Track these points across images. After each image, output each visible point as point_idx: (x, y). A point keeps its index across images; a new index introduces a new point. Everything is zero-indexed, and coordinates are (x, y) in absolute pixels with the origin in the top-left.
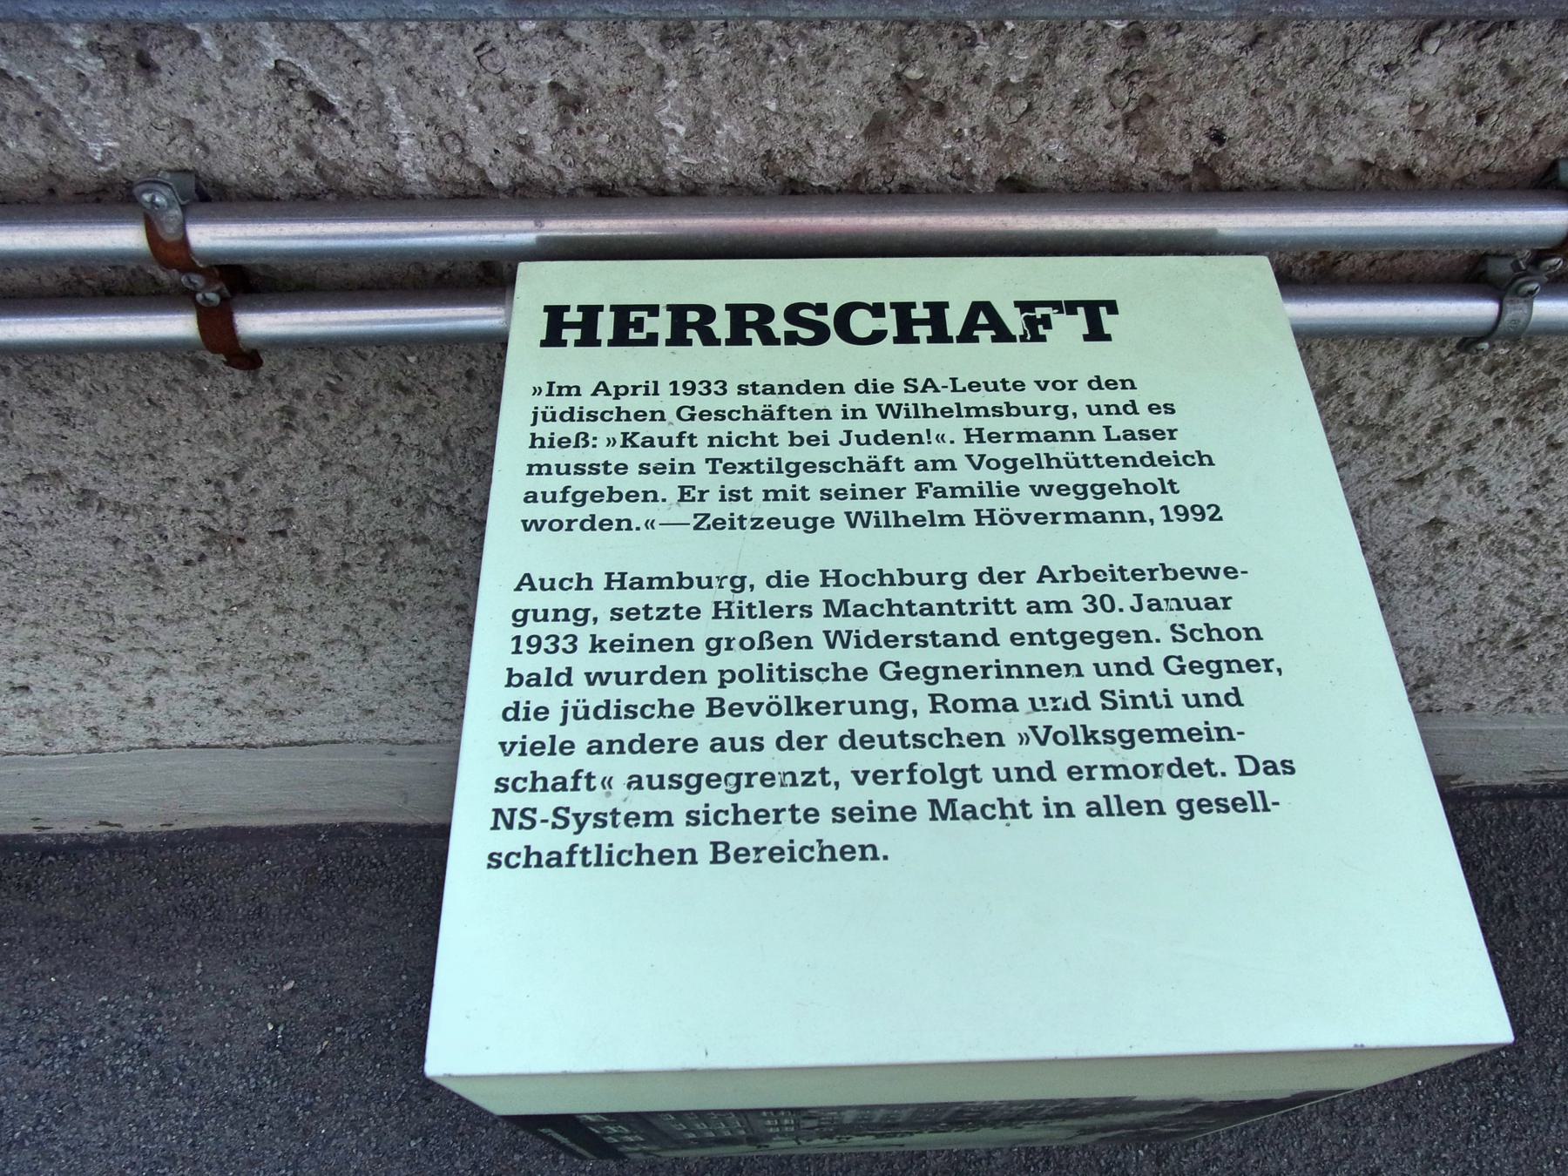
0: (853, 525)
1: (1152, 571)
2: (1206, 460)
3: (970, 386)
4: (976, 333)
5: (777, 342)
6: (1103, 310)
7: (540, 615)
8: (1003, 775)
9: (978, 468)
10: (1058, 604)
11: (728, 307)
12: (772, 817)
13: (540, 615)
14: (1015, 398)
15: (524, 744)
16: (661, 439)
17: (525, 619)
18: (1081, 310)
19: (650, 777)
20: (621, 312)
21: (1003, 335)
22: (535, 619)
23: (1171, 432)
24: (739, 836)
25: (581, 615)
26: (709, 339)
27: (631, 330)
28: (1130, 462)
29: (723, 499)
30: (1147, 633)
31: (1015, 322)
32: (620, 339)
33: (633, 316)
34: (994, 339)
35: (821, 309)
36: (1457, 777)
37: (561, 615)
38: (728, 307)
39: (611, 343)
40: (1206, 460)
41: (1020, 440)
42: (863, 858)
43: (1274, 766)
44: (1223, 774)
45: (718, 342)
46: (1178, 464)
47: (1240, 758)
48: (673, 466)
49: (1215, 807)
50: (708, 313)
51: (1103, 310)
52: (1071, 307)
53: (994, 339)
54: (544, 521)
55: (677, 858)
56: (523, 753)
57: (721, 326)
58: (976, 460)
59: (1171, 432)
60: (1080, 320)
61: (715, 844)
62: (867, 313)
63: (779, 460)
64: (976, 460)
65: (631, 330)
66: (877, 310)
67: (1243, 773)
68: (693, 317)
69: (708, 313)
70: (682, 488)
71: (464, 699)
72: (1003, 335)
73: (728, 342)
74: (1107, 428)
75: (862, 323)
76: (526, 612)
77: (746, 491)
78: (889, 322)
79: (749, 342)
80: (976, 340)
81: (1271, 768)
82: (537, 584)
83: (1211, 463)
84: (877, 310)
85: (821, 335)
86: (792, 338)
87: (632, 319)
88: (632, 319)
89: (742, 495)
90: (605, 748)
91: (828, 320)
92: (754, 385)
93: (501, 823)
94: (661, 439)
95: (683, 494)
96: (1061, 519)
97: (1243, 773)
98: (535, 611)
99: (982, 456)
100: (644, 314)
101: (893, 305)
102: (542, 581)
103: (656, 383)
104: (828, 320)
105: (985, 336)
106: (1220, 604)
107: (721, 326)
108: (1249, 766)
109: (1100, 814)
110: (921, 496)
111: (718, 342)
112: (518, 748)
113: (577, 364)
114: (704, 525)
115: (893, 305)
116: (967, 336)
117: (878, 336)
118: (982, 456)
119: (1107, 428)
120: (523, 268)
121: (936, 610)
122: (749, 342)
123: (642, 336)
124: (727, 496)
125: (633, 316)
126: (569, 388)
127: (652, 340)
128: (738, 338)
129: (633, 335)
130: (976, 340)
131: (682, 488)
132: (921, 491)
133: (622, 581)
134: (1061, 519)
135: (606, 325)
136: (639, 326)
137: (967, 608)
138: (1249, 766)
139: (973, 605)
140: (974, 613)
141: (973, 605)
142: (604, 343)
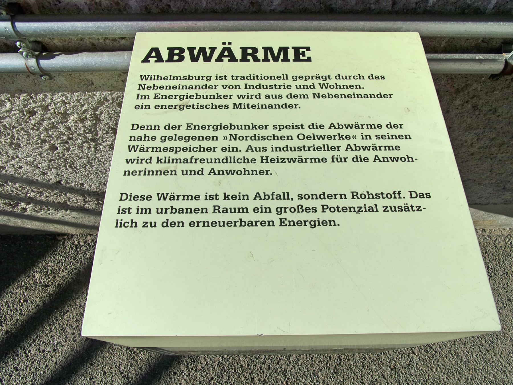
1: (334, 136)
4: (223, 58)
8: (185, 173)
10: (389, 147)
11: (263, 48)
12: (303, 224)
16: (272, 95)
19: (231, 209)
20: (296, 49)
21: (233, 59)
26: (256, 59)
27: (301, 56)
31: (238, 55)
32: (297, 59)
33: (301, 51)
34: (229, 61)
38: (263, 48)
39: (294, 60)
42: (269, 225)
43: (423, 195)
44: (404, 198)
45: (259, 61)
47: (410, 192)
48: (259, 105)
49: (311, 210)
50: (255, 50)
53: (229, 61)
54: (226, 86)
55: (267, 224)
57: (260, 55)
61: (214, 206)
65: (301, 56)
67: (411, 197)
68: (250, 51)
69: (255, 50)
72: (233, 59)
73: (241, 61)
79: (248, 61)
80: (222, 61)
81: (422, 196)
82: (254, 149)
87: (301, 52)
88: (301, 52)
90: (185, 211)
94: (272, 95)
96: (309, 161)
97: (411, 197)
100: (305, 50)
102: (256, 148)
103: (287, 75)
105: (226, 59)
107: (260, 55)
108: (414, 195)
109: (373, 211)
111: (259, 61)
113: (154, 68)
120: (138, 34)
121: (274, 107)
122: (248, 61)
123: (305, 58)
125: (301, 51)
126: (177, 77)
128: (244, 59)
129: (302, 57)
130: (222, 61)
133: (267, 160)
134: (309, 161)
135: (291, 54)
136: (303, 54)
137: (307, 149)
138: (414, 195)
139: (280, 86)
140: (309, 150)
141: (280, 86)
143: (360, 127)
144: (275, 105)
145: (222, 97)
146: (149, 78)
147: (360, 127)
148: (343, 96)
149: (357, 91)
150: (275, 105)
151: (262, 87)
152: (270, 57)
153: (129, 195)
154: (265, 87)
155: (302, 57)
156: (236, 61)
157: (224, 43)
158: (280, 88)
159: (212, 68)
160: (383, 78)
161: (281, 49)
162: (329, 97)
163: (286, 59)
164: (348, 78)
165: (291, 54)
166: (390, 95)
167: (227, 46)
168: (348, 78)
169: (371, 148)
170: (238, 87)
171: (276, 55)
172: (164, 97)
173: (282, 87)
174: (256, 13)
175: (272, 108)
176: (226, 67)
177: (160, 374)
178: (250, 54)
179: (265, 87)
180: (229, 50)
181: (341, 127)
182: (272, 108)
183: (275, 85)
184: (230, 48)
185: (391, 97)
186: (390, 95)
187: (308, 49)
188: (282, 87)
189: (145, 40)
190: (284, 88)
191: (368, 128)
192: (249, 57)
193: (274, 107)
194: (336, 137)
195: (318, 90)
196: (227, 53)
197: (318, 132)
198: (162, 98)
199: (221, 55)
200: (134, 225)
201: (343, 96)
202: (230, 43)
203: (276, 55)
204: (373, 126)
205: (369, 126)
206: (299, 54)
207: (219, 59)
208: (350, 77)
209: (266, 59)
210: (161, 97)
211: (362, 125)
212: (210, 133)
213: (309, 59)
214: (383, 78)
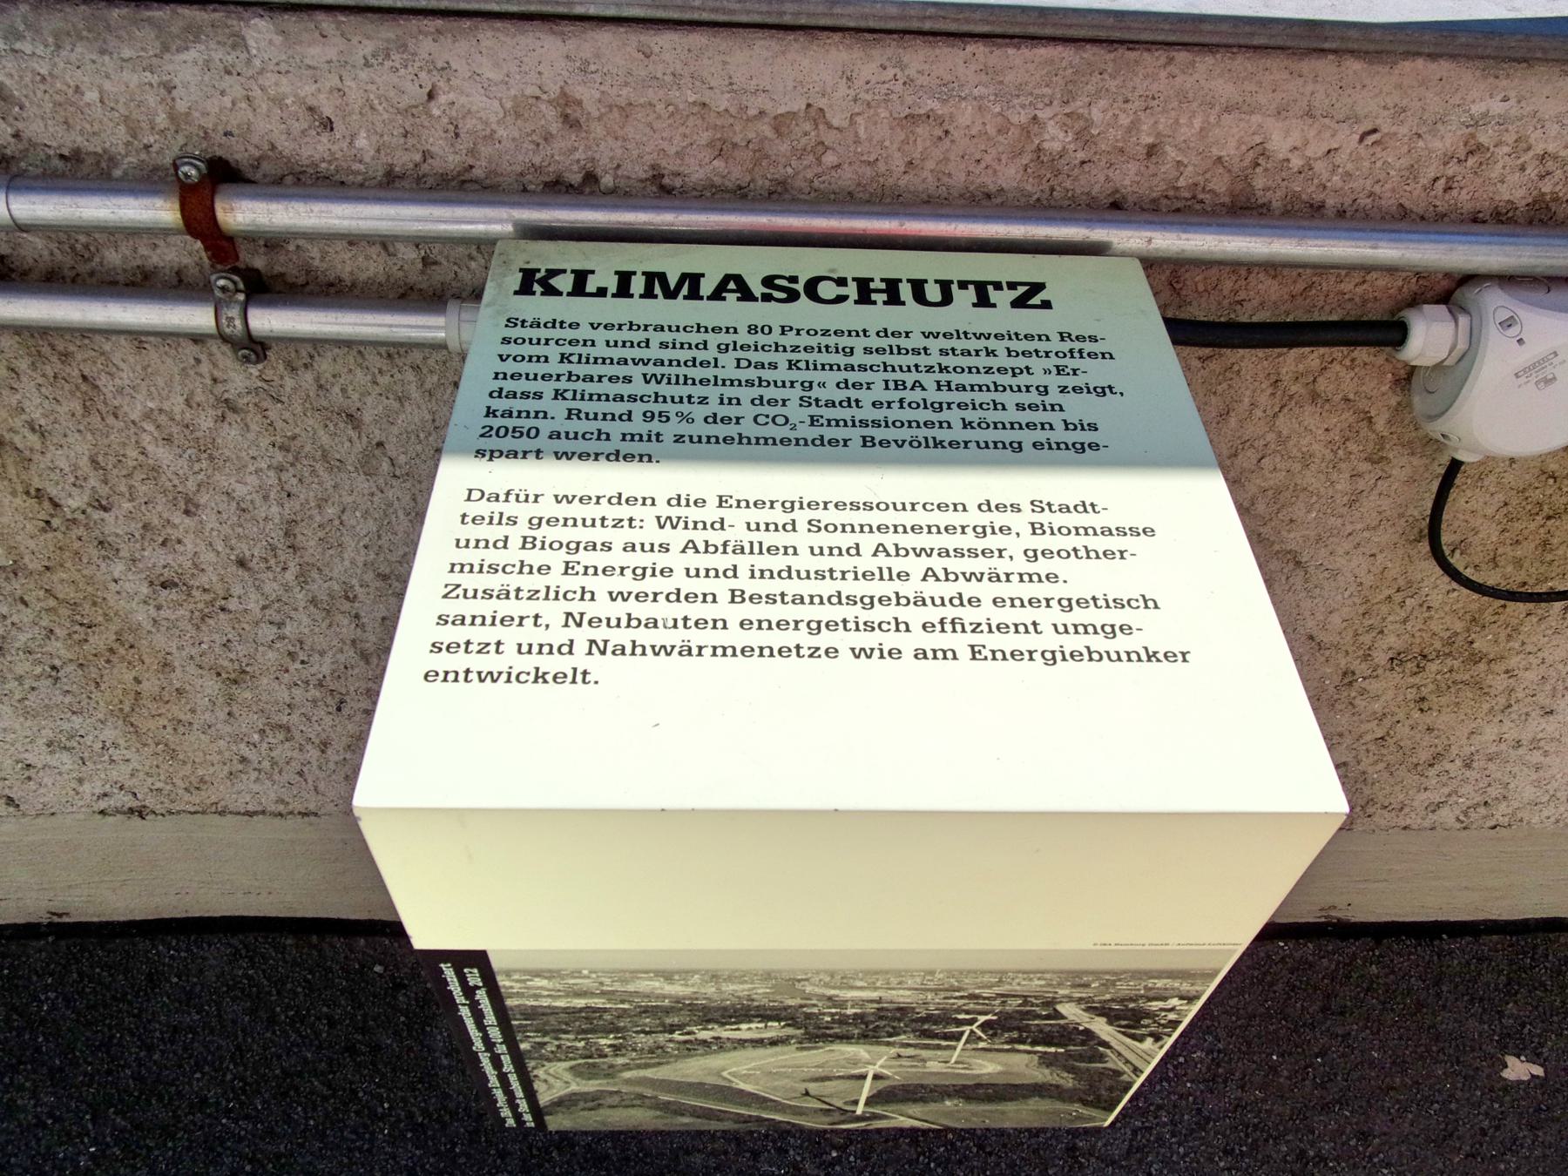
2: (1151, 604)
5: (756, 299)
6: (990, 288)
15: (509, 674)
18: (971, 287)
23: (1184, 654)
24: (879, 434)
28: (1017, 603)
35: (794, 279)
38: (903, 303)
40: (1151, 604)
51: (990, 288)
52: (963, 285)
56: (509, 681)
59: (1184, 654)
60: (971, 294)
62: (833, 284)
66: (842, 282)
71: (373, 695)
73: (642, 296)
75: (827, 290)
78: (852, 290)
83: (1156, 607)
84: (842, 282)
85: (793, 296)
86: (767, 298)
91: (800, 287)
93: (594, 649)
101: (854, 279)
104: (800, 287)
112: (504, 677)
114: (453, 594)
115: (854, 279)
116: (717, 295)
117: (841, 299)
121: (807, 600)
127: (602, 292)
139: (843, 573)
141: (843, 573)
142: (636, 296)
143: (1003, 578)
144: (812, 597)
145: (549, 678)
146: (682, 524)
147: (1003, 578)
148: (934, 530)
150: (812, 597)
151: (794, 574)
152: (658, 290)
154: (803, 575)
158: (843, 578)
161: (684, 277)
162: (1091, 659)
164: (909, 507)
168: (909, 507)
169: (986, 577)
170: (709, 598)
172: (591, 571)
173: (850, 576)
174: (981, 1139)
175: (802, 602)
176: (732, 310)
179: (803, 575)
181: (952, 577)
182: (802, 602)
183: (831, 571)
188: (850, 576)
190: (856, 578)
191: (1022, 580)
193: (807, 600)
195: (744, 582)
197: (761, 339)
198: (586, 573)
200: (588, 596)
201: (934, 530)
204: (1035, 578)
205: (1026, 578)
208: (913, 505)
209: (648, 294)
210: (582, 571)
211: (1008, 575)
212: (779, 516)
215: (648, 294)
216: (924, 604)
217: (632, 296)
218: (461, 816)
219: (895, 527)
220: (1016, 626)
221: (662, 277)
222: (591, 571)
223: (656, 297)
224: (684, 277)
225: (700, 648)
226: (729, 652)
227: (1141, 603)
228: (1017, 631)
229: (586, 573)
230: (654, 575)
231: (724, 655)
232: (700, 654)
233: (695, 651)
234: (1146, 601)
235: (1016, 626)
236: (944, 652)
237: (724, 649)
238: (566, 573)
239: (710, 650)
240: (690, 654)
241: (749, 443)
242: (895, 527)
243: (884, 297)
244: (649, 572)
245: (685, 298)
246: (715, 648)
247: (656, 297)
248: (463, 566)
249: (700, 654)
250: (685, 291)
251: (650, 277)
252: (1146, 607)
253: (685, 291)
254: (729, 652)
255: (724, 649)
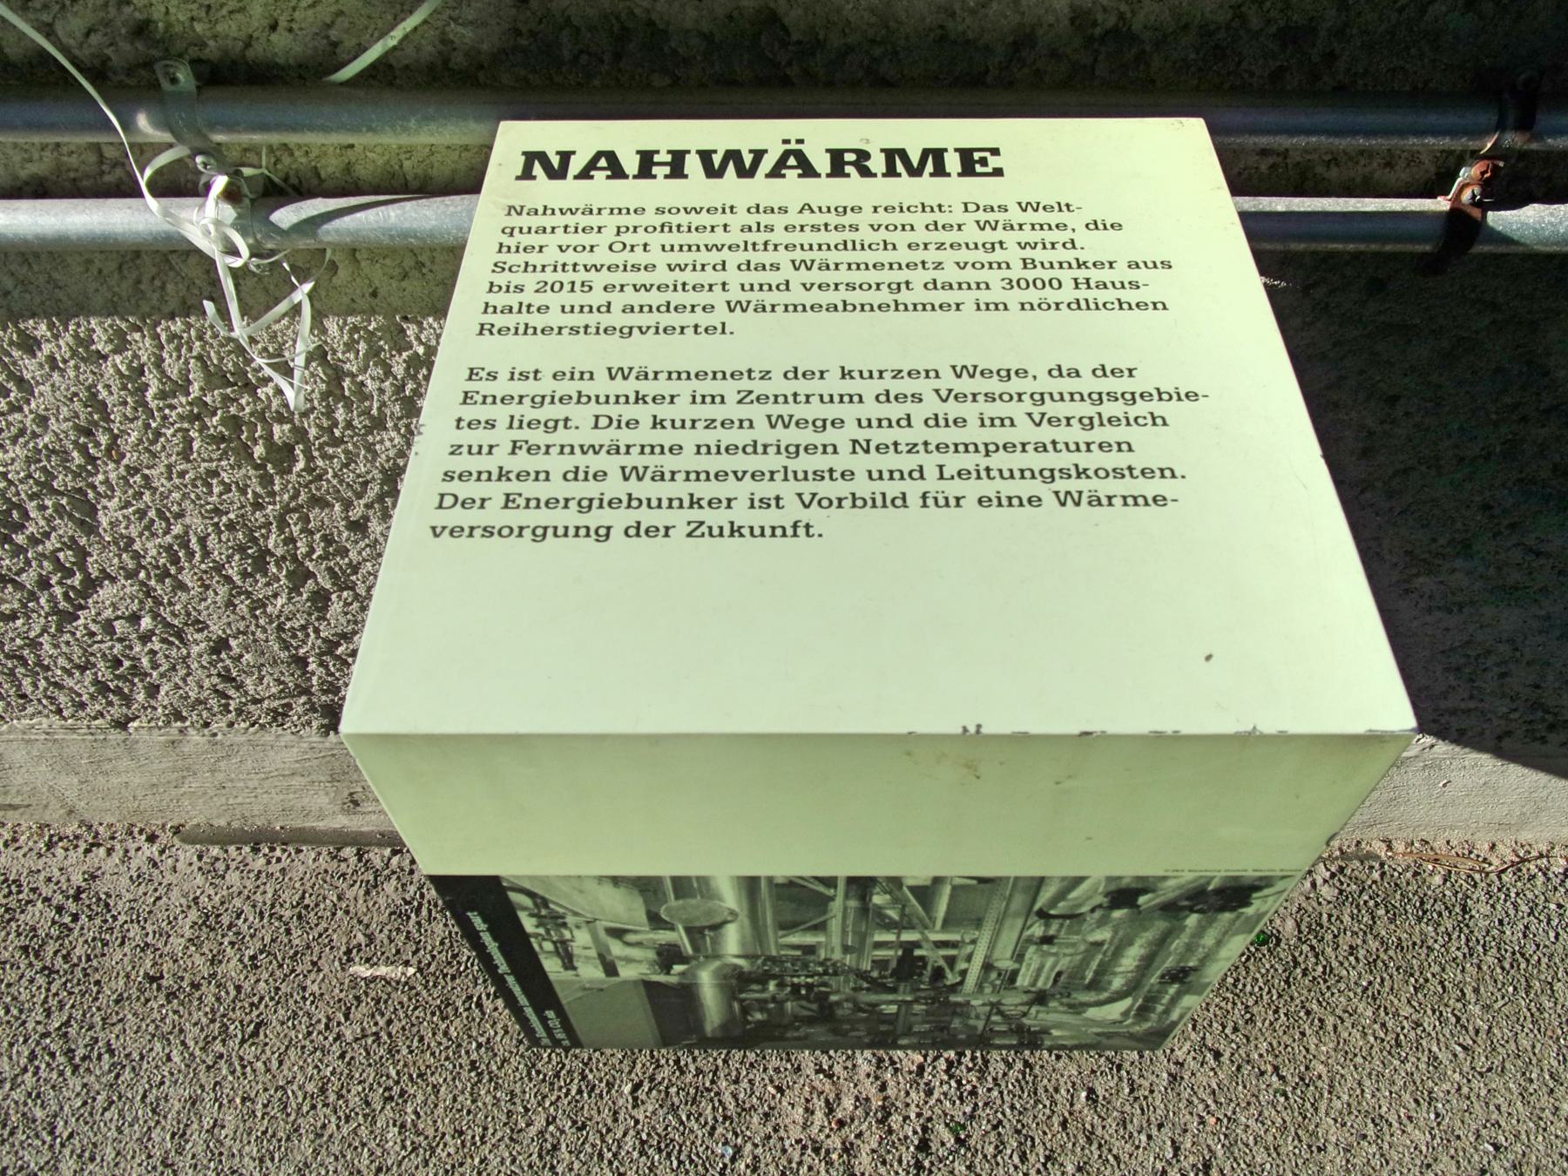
0: (1063, 504)
2: (1159, 421)
3: (959, 474)
7: (561, 532)
9: (807, 506)
13: (561, 532)
14: (588, 388)
17: (544, 535)
22: (555, 535)
25: (602, 531)
26: (865, 172)
29: (752, 506)
30: (1172, 471)
31: (822, 163)
33: (977, 156)
36: (1208, 883)
37: (582, 532)
41: (688, 479)
46: (1179, 399)
50: (863, 155)
57: (877, 163)
58: (807, 499)
63: (884, 495)
64: (807, 499)
70: (508, 495)
73: (884, 175)
74: (941, 467)
76: (545, 528)
77: (778, 499)
83: (1165, 424)
89: (773, 503)
92: (831, 471)
95: (508, 500)
96: (1117, 501)
98: (556, 528)
99: (814, 495)
100: (987, 154)
105: (792, 174)
106: (1105, 501)
110: (513, 453)
111: (875, 175)
118: (814, 495)
119: (941, 467)
123: (989, 170)
124: (757, 504)
125: (977, 156)
129: (978, 169)
130: (592, 177)
131: (508, 495)
132: (514, 447)
134: (1117, 501)
135: (953, 162)
136: (984, 162)
149: (1130, 296)
152: (900, 168)
153: (615, 418)
155: (978, 169)
156: (625, 176)
157: (786, 142)
159: (760, 188)
160: (1167, 265)
163: (940, 171)
165: (953, 162)
166: (1130, 371)
167: (793, 146)
171: (731, 164)
176: (601, 188)
177: (1219, 892)
178: (850, 163)
180: (799, 155)
184: (800, 151)
185: (1131, 375)
186: (1130, 371)
187: (995, 152)
189: (516, 137)
191: (1125, 504)
192: (848, 169)
194: (844, 503)
196: (796, 161)
199: (781, 164)
202: (800, 141)
203: (731, 164)
205: (1130, 501)
206: (970, 162)
207: (776, 173)
209: (891, 172)
213: (998, 172)
214: (1167, 265)
215: (891, 172)
216: (1045, 450)
217: (949, 175)
218: (908, 743)
219: (927, 372)
220: (1162, 470)
221: (903, 154)
222: (489, 400)
223: (899, 175)
224: (926, 153)
225: (673, 473)
226: (703, 476)
227: (1149, 421)
228: (1163, 476)
229: (484, 402)
230: (552, 402)
231: (698, 479)
232: (673, 479)
233: (668, 476)
234: (1154, 419)
235: (1162, 470)
236: (1135, 498)
237: (698, 474)
238: (465, 402)
239: (683, 475)
240: (662, 479)
241: (906, 309)
242: (927, 372)
243: (657, 158)
244: (548, 399)
245: (932, 175)
246: (688, 473)
247: (899, 175)
248: (653, 447)
249: (673, 479)
250: (929, 167)
251: (890, 154)
252: (1154, 424)
253: (929, 167)
254: (703, 476)
255: (698, 474)
